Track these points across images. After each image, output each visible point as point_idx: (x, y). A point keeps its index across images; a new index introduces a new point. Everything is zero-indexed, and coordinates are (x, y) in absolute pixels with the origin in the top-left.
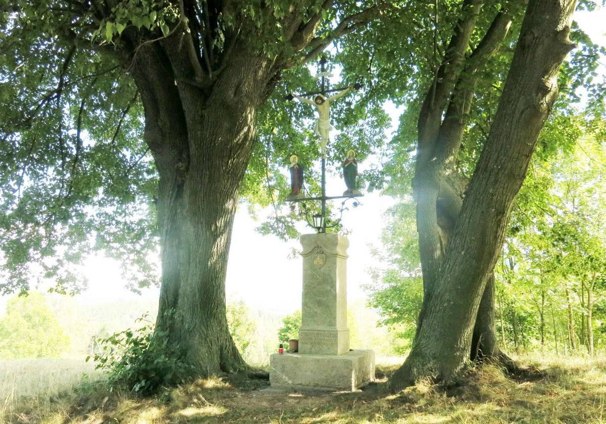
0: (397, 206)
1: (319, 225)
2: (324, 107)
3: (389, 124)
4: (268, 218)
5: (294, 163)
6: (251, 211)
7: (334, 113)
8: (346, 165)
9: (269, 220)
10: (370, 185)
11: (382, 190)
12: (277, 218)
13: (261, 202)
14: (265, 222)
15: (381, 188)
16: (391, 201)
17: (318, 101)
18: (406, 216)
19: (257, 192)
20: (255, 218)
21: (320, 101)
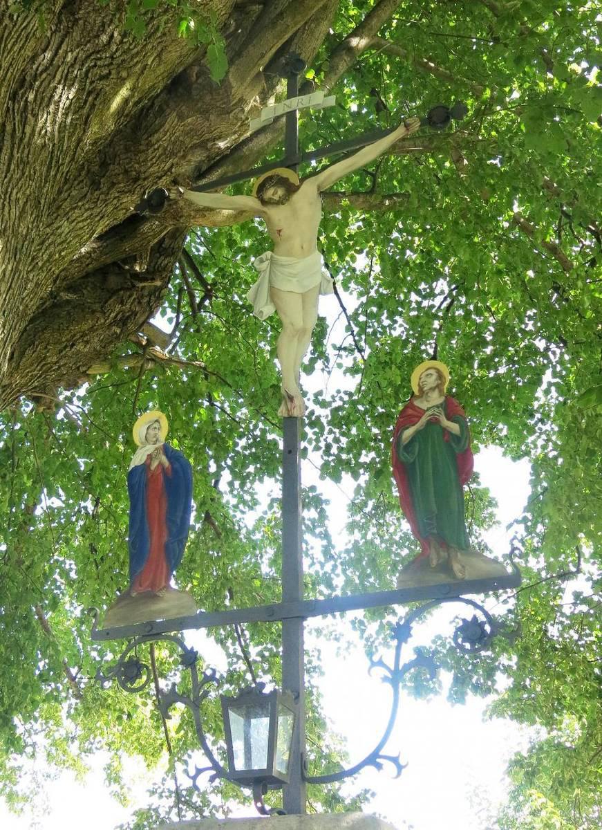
0: (538, 749)
1: (259, 763)
2: (295, 212)
3: (491, 515)
4: (153, 793)
5: (150, 448)
6: (113, 777)
7: (341, 449)
8: (408, 433)
9: (155, 801)
10: (456, 679)
11: (492, 697)
12: (178, 793)
13: (142, 750)
14: (144, 806)
15: (488, 691)
16: (523, 736)
17: (269, 193)
18: (571, 783)
19: (129, 716)
20: (122, 799)
21: (280, 192)
